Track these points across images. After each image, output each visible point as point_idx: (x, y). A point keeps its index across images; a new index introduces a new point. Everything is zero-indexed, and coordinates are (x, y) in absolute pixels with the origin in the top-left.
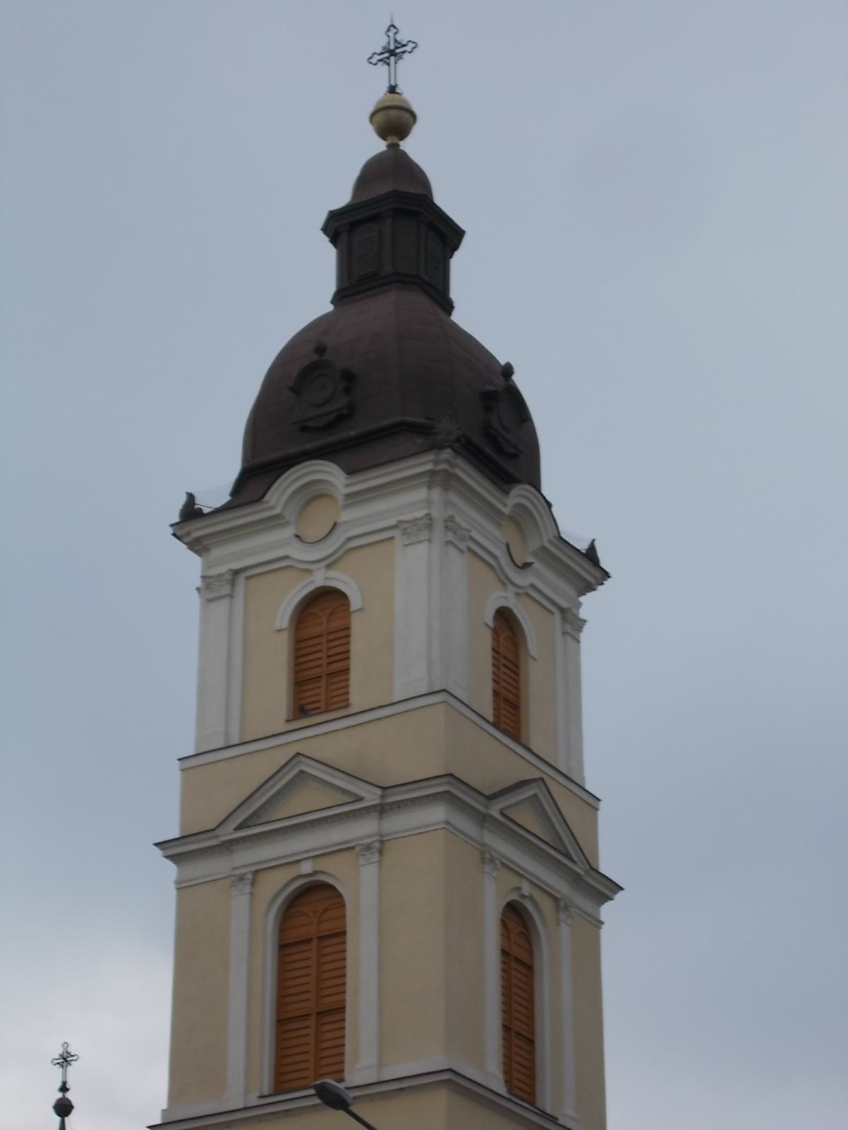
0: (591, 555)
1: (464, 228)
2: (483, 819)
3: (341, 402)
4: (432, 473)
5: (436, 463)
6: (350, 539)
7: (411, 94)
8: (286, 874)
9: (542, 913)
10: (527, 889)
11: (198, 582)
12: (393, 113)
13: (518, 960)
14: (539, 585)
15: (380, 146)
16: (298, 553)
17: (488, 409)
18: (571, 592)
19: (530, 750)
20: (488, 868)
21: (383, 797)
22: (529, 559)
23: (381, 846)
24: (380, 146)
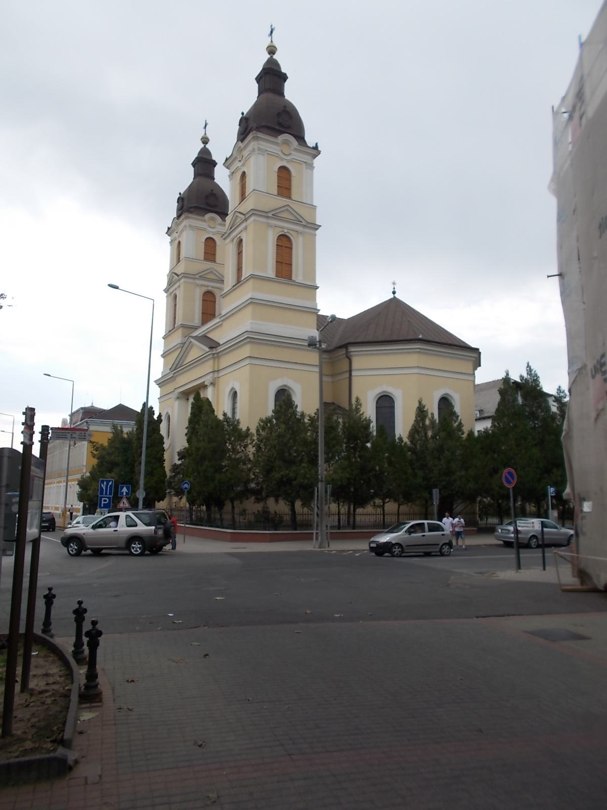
0: (316, 148)
4: (253, 137)
5: (253, 135)
7: (276, 43)
8: (236, 238)
12: (272, 48)
14: (295, 158)
20: (269, 228)
23: (246, 228)
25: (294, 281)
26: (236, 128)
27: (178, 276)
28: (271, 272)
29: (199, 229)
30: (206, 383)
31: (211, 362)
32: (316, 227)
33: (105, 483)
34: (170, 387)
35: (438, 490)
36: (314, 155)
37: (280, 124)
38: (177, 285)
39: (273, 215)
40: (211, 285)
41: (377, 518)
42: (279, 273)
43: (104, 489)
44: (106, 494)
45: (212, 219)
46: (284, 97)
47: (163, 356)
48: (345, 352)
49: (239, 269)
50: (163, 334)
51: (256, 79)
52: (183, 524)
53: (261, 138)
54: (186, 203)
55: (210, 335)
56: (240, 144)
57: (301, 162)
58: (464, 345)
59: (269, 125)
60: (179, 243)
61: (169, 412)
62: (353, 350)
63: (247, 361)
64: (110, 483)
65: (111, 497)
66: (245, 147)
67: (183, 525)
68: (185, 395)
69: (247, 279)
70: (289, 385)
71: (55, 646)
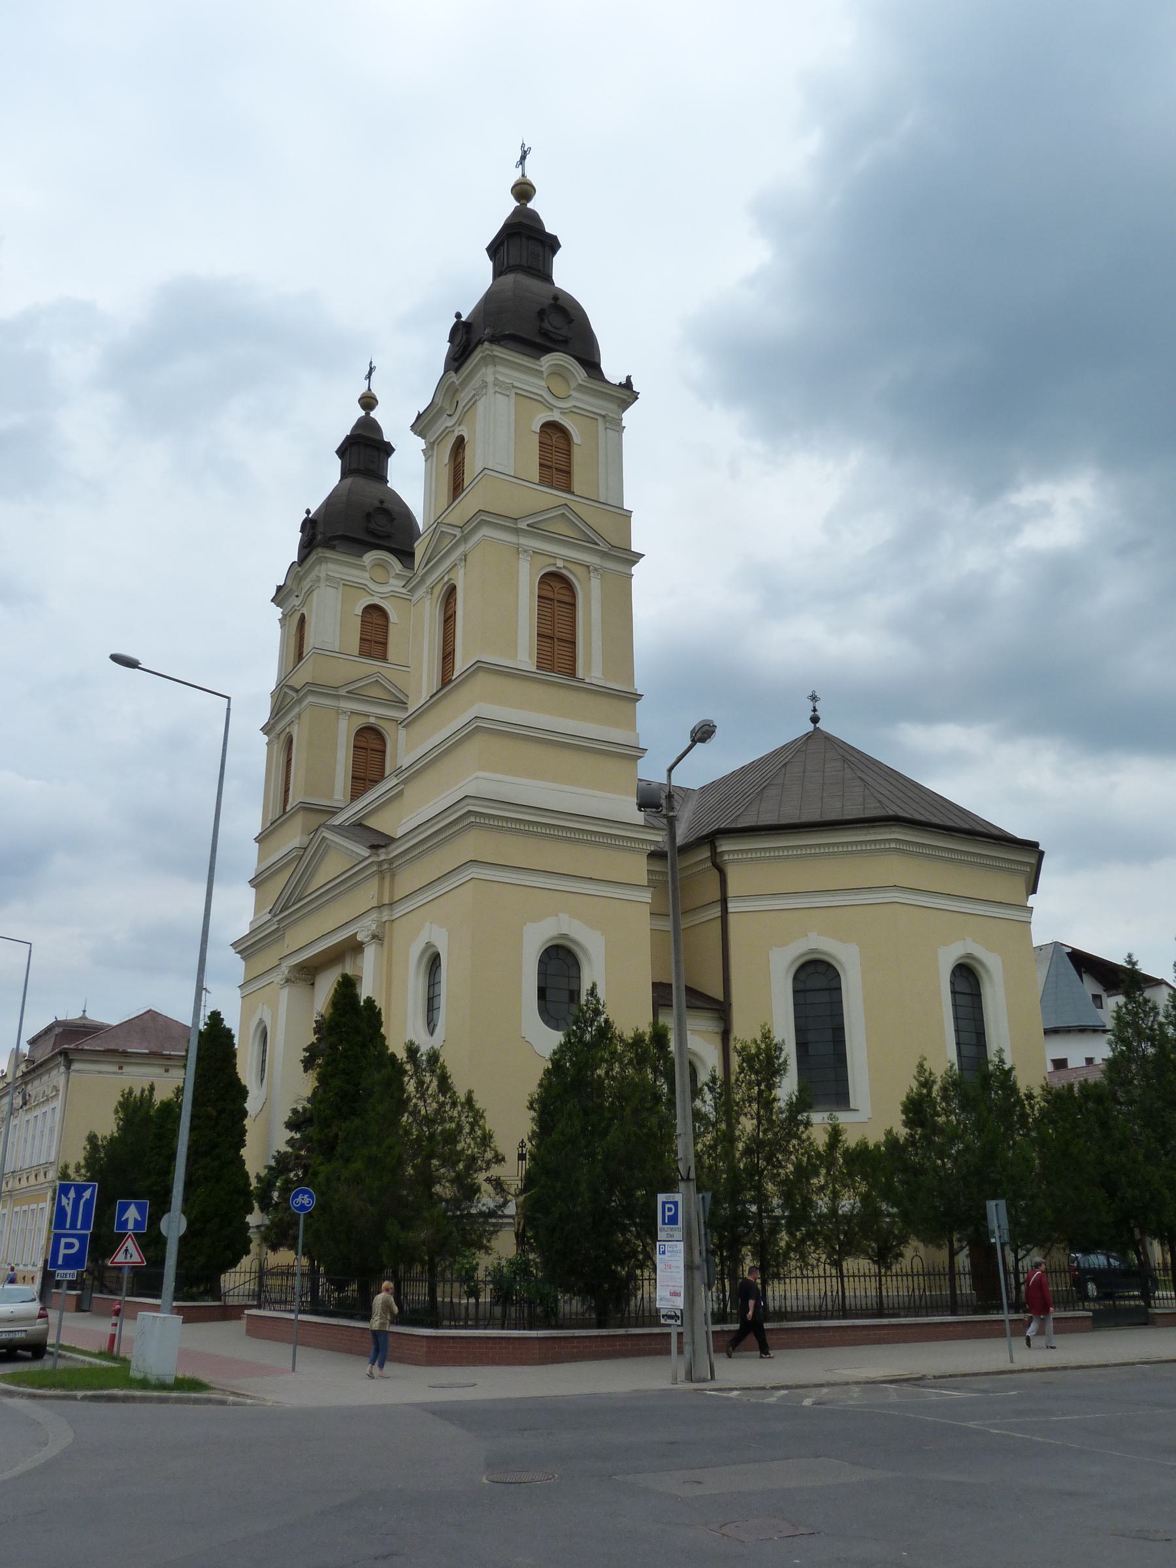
0: (628, 385)
7: (531, 177)
21: (462, 532)
25: (582, 681)
26: (442, 348)
27: (297, 691)
28: (525, 656)
29: (347, 585)
30: (359, 938)
31: (374, 884)
33: (72, 1194)
34: (268, 958)
35: (1002, 1203)
36: (624, 400)
37: (373, 533)
38: (297, 710)
39: (528, 525)
40: (374, 713)
41: (828, 1288)
42: (546, 661)
43: (69, 1210)
44: (73, 1226)
45: (381, 565)
46: (554, 284)
47: (257, 840)
48: (709, 854)
49: (448, 656)
50: (257, 830)
51: (488, 249)
52: (291, 1311)
53: (502, 358)
54: (320, 529)
55: (371, 823)
56: (453, 377)
58: (996, 832)
60: (302, 619)
61: (264, 1018)
62: (724, 848)
64: (87, 1195)
65: (86, 1235)
66: (464, 383)
67: (292, 1316)
68: (308, 972)
70: (573, 934)
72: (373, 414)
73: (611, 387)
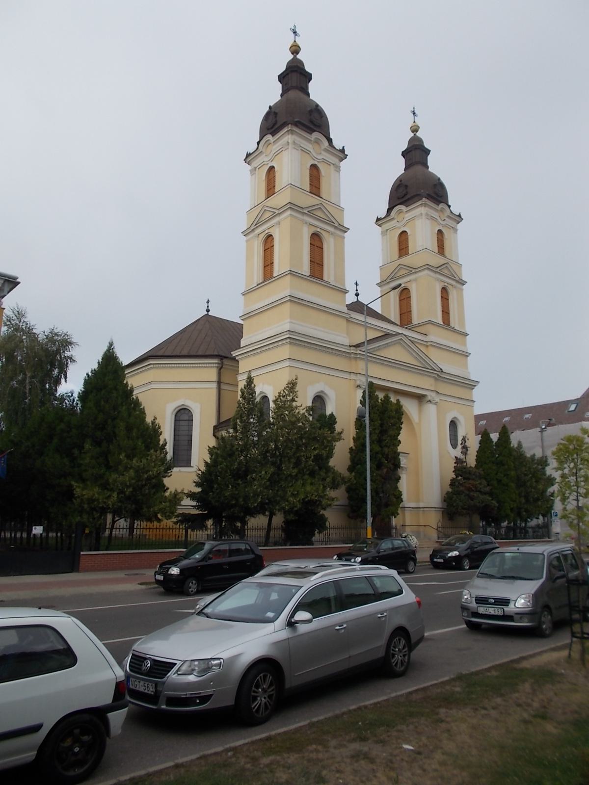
0: (459, 216)
1: (310, 72)
2: (436, 272)
3: (405, 192)
4: (288, 131)
6: (275, 153)
9: (450, 289)
10: (446, 284)
11: (381, 233)
13: (445, 298)
15: (412, 135)
16: (398, 225)
17: (311, 115)
18: (456, 224)
19: (321, 198)
22: (445, 218)
23: (279, 223)
24: (292, 57)
28: (306, 269)
32: (345, 230)
37: (312, 122)
39: (308, 211)
57: (328, 163)
59: (302, 121)
63: (287, 363)
69: (282, 276)
71: (266, 658)
72: (298, 56)
73: (336, 151)
